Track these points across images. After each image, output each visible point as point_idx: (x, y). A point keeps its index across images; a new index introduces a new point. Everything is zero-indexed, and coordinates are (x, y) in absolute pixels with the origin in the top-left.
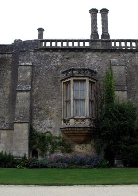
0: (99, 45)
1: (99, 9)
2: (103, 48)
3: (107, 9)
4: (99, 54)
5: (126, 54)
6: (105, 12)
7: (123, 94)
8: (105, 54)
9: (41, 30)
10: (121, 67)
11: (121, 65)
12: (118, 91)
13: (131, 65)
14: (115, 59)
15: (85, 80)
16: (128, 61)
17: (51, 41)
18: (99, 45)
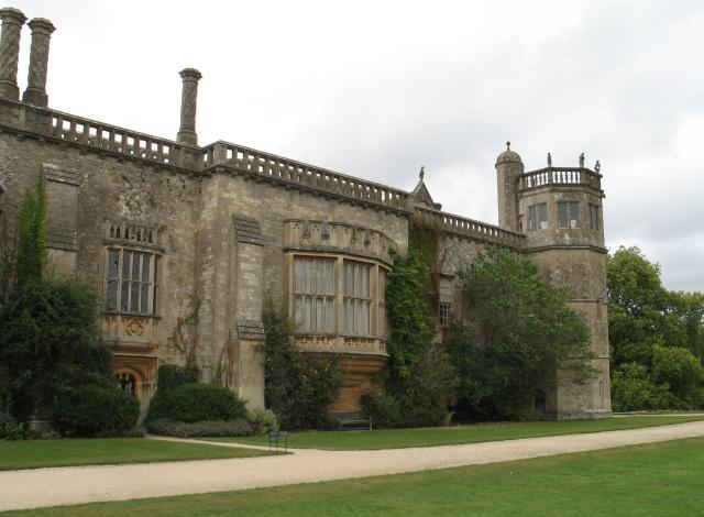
0: (17, 117)
1: (30, 17)
2: (28, 129)
5: (82, 157)
6: (43, 29)
7: (67, 259)
8: (30, 145)
9: (508, 144)
10: (69, 188)
11: (70, 184)
12: (56, 249)
13: (91, 186)
14: (54, 163)
16: (86, 176)
17: (62, 117)
18: (17, 117)
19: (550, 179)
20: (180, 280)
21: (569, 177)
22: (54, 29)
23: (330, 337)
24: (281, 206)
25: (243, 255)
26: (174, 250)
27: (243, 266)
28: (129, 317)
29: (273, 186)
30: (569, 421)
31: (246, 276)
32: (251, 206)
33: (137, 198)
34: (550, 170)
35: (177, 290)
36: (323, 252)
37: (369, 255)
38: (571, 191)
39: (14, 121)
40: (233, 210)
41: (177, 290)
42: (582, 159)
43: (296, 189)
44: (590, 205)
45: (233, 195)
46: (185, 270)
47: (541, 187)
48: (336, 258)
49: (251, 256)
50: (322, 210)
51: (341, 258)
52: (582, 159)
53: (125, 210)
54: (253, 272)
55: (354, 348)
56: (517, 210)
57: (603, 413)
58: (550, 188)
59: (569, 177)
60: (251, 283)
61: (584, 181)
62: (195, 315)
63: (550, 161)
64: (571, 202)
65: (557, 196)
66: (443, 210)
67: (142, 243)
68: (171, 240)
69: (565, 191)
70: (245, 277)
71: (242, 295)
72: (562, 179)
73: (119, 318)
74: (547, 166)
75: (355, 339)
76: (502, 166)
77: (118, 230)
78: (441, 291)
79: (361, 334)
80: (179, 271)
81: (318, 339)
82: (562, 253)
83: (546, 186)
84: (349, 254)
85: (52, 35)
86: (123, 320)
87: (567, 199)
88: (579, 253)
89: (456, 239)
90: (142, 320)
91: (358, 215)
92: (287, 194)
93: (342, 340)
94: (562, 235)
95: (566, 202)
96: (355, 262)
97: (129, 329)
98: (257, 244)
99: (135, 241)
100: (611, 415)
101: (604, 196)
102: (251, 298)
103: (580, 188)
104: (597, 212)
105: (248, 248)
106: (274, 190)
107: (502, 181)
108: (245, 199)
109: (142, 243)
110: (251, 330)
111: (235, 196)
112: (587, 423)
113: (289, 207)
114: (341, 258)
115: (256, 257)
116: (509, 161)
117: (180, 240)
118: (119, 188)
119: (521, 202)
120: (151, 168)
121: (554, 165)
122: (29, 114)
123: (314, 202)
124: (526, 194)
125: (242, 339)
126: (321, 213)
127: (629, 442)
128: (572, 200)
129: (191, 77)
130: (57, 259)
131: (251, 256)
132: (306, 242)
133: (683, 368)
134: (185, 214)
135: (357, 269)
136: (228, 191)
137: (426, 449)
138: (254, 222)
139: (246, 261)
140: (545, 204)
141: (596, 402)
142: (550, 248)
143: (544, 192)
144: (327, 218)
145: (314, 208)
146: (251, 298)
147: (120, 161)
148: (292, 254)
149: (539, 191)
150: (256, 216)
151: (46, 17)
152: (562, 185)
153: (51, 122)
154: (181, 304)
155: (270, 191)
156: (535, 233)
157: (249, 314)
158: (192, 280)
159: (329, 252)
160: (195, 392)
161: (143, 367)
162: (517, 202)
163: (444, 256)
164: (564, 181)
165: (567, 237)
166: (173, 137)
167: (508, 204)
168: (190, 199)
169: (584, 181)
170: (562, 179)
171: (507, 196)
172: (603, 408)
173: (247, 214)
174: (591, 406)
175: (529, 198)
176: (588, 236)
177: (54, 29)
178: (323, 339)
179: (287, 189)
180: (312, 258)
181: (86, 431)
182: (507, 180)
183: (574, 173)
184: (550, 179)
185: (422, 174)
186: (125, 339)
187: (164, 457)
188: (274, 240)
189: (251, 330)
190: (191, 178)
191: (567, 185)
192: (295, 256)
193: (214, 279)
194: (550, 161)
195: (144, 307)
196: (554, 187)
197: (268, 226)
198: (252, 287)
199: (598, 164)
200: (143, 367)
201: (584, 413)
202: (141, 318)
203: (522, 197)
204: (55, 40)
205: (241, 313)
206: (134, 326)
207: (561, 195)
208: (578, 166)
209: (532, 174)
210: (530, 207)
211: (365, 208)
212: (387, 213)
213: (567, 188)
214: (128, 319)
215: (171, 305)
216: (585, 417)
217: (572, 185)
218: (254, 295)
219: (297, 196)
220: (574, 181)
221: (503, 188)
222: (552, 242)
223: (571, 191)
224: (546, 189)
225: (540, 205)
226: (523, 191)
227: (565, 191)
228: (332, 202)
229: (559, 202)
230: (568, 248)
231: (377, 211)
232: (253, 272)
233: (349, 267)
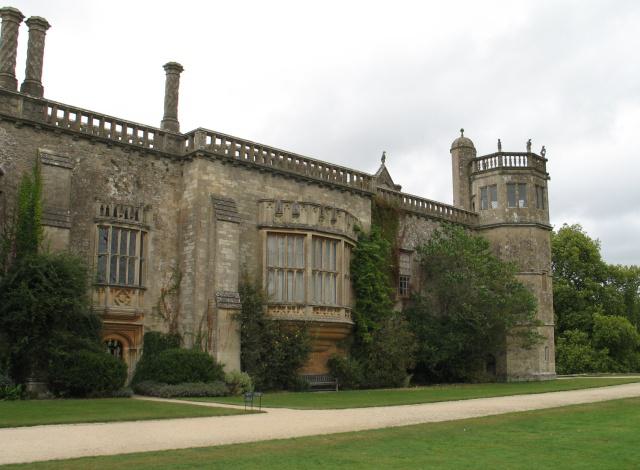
0: (15, 106)
1: (28, 15)
2: (26, 117)
3: (20, 13)
4: (13, 128)
5: (74, 143)
6: (39, 26)
7: (61, 235)
8: (27, 131)
9: (462, 131)
10: (63, 171)
11: (64, 167)
12: (51, 226)
13: (83, 169)
14: (49, 149)
15: (108, 227)
17: (56, 106)
18: (15, 106)
19: (500, 163)
20: (164, 255)
21: (517, 161)
22: (49, 26)
23: (300, 306)
24: (256, 187)
25: (221, 232)
26: (158, 227)
27: (221, 242)
28: (117, 288)
29: (248, 169)
30: (517, 383)
31: (224, 251)
32: (228, 187)
33: (125, 180)
34: (500, 154)
35: (161, 264)
36: (293, 229)
37: (336, 232)
38: (519, 174)
39: (13, 110)
40: (211, 191)
41: (161, 264)
42: (529, 144)
43: (269, 172)
44: (537, 186)
45: (212, 177)
46: (168, 246)
47: (492, 170)
48: (306, 235)
49: (229, 233)
50: (293, 191)
51: (310, 234)
52: (529, 144)
53: (114, 191)
54: (230, 247)
55: (321, 317)
56: (470, 191)
57: (548, 376)
58: (500, 171)
59: (517, 161)
60: (228, 257)
61: (531, 165)
62: (177, 287)
63: (500, 146)
64: (519, 184)
65: (507, 178)
66: (403, 191)
67: (129, 221)
68: (156, 218)
69: (514, 174)
70: (223, 252)
71: (220, 268)
72: (511, 163)
73: (108, 289)
74: (497, 151)
75: (323, 308)
76: (456, 151)
77: (108, 209)
78: (401, 265)
79: (328, 304)
80: (163, 247)
81: (289, 308)
82: (511, 230)
83: (496, 169)
84: (318, 231)
85: (47, 32)
86: (112, 291)
87: (516, 181)
88: (527, 230)
89: (415, 218)
90: (129, 291)
91: (326, 195)
92: (261, 177)
93: (311, 309)
94: (511, 213)
95: (515, 184)
96: (322, 238)
97: (117, 299)
98: (234, 222)
99: (122, 219)
100: (555, 378)
101: (549, 178)
102: (228, 271)
103: (528, 171)
104: (543, 193)
105: (226, 225)
106: (249, 173)
107: (457, 164)
108: (223, 181)
109: (129, 221)
110: (228, 300)
111: (214, 179)
112: (534, 385)
113: (263, 188)
114: (310, 234)
115: (233, 234)
116: (463, 147)
117: (164, 218)
118: (108, 171)
119: (474, 184)
120: (137, 153)
121: (503, 150)
122: (27, 103)
123: (286, 183)
124: (478, 176)
125: (220, 308)
126: (292, 194)
127: (572, 402)
128: (520, 182)
129: (174, 70)
130: (52, 235)
131: (229, 233)
132: (278, 220)
133: (621, 335)
134: (168, 195)
135: (324, 244)
136: (208, 174)
137: (387, 408)
138: (231, 201)
139: (224, 237)
140: (495, 185)
141: (542, 365)
142: (500, 226)
143: (495, 175)
144: (297, 198)
145: (285, 189)
146: (228, 271)
147: (109, 146)
148: (265, 231)
149: (490, 173)
150: (232, 196)
151: (42, 15)
152: (511, 168)
153: (47, 111)
154: (164, 276)
155: (246, 173)
156: (486, 212)
157: (227, 285)
158: (174, 254)
159: (299, 229)
160: (177, 357)
161: (130, 334)
162: (470, 183)
163: (404, 233)
164: (513, 165)
165: (515, 215)
166: (157, 124)
167: (462, 186)
168: (172, 181)
169: (531, 165)
170: (511, 163)
171: (461, 178)
172: (548, 371)
173: (224, 194)
174: (537, 370)
175: (481, 180)
176: (535, 214)
177: (49, 26)
178: (294, 308)
179: (261, 172)
180: (283, 235)
181: (78, 392)
182: (461, 164)
183: (522, 158)
184: (500, 163)
185: (383, 159)
186: (114, 309)
187: (149, 415)
188: (249, 218)
189: (228, 300)
190: (173, 162)
191: (515, 168)
192: (268, 233)
193: (195, 253)
194: (500, 146)
195: (131, 279)
196: (503, 170)
197: (244, 205)
198: (229, 261)
199: (543, 149)
200: (130, 334)
201: (531, 376)
202: (129, 289)
203: (474, 179)
204: (50, 37)
205: (219, 285)
206: (122, 297)
207: (510, 177)
208: (525, 151)
209: (483, 158)
210: (482, 188)
211: (332, 189)
212: (352, 194)
213: (515, 171)
214: (117, 290)
215: (156, 277)
216: (532, 379)
217: (520, 168)
218: (231, 268)
219: (270, 178)
220: (522, 165)
221: (457, 171)
222: (501, 220)
223: (519, 174)
224: (497, 172)
225: (491, 186)
226: (475, 174)
227: (514, 174)
228: (302, 184)
229: (508, 184)
230: (517, 226)
231: (342, 192)
232: (230, 247)
233: (317, 243)
